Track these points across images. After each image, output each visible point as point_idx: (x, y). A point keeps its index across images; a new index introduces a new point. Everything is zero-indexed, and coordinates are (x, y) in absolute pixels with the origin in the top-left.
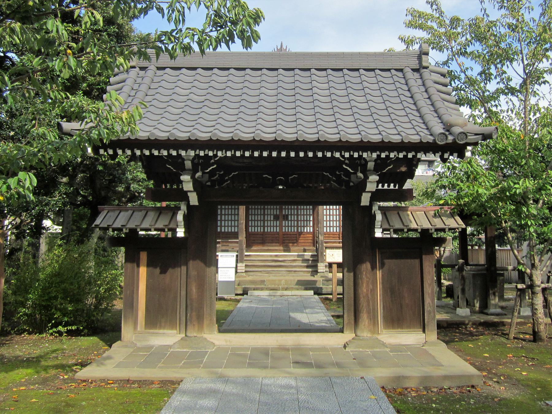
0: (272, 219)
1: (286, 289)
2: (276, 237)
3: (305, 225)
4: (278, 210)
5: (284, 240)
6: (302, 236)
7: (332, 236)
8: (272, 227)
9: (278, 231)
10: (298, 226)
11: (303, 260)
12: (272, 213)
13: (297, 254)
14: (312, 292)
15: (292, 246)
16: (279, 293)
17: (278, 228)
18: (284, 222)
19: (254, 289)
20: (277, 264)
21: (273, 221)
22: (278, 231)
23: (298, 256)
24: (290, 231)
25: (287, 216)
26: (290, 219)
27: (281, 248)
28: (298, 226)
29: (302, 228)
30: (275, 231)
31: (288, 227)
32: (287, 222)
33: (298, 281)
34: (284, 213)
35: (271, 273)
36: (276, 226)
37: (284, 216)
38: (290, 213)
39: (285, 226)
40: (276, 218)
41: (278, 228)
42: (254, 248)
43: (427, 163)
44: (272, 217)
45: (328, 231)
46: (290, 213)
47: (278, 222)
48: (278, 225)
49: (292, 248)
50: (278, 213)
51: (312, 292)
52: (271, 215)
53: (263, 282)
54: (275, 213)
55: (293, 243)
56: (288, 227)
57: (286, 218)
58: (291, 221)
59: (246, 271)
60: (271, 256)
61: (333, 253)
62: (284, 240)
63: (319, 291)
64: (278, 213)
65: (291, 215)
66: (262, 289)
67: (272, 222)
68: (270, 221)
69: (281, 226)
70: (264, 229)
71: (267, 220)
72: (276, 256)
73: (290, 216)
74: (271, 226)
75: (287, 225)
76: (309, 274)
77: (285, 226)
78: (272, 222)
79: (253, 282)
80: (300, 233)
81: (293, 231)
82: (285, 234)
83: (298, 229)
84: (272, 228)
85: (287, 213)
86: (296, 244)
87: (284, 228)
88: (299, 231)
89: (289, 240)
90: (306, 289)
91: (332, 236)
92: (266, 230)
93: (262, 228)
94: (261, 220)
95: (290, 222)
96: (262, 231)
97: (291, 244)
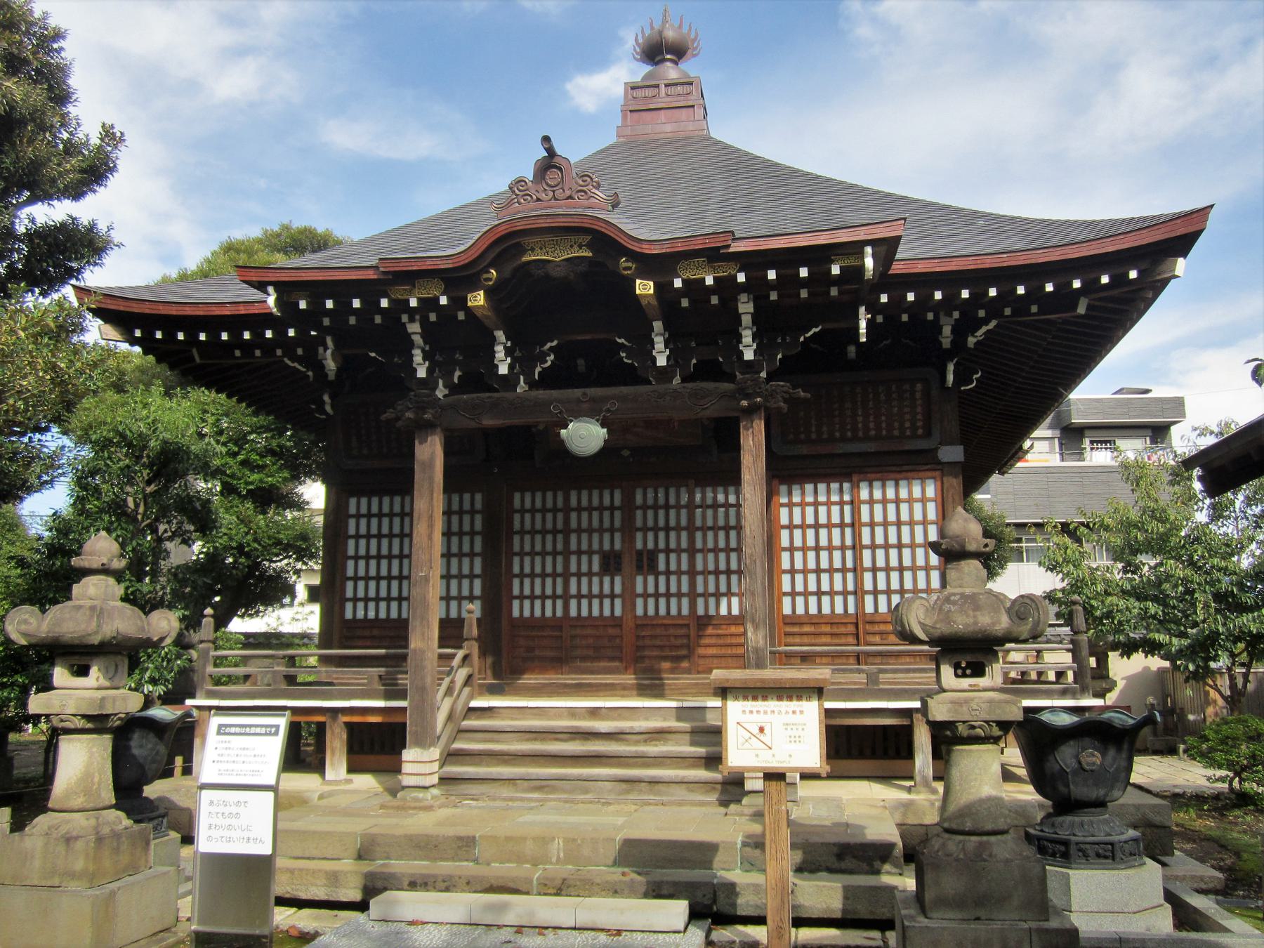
0: (596, 568)
1: (561, 889)
2: (612, 638)
3: (723, 589)
4: (617, 536)
5: (639, 648)
6: (710, 631)
7: (827, 629)
8: (596, 599)
9: (618, 612)
10: (693, 595)
11: (693, 732)
12: (596, 546)
13: (674, 704)
14: (679, 909)
15: (672, 671)
16: (520, 908)
17: (618, 602)
18: (639, 579)
19: (413, 885)
20: (590, 749)
21: (601, 575)
22: (618, 612)
23: (681, 713)
24: (662, 611)
25: (652, 556)
26: (662, 567)
27: (629, 679)
28: (693, 595)
29: (712, 601)
30: (596, 613)
31: (656, 597)
32: (651, 579)
33: (629, 844)
34: (639, 545)
35: (554, 790)
36: (612, 596)
37: (640, 554)
38: (662, 545)
39: (645, 596)
40: (611, 563)
41: (618, 602)
42: (529, 679)
43: (1149, 432)
44: (596, 559)
45: (813, 610)
46: (662, 545)
47: (618, 580)
48: (618, 590)
49: (670, 680)
50: (618, 546)
51: (679, 909)
52: (590, 553)
53: (465, 845)
54: (607, 547)
55: (678, 659)
56: (656, 597)
57: (646, 563)
58: (668, 573)
59: (444, 780)
60: (572, 713)
61: (761, 719)
62: (639, 648)
63: (722, 906)
64: (618, 546)
65: (668, 551)
66: (448, 885)
67: (596, 580)
68: (590, 574)
69: (629, 596)
70: (566, 607)
71: (579, 575)
72: (594, 713)
73: (662, 557)
74: (657, 595)
75: (651, 590)
76: (713, 797)
77: (645, 596)
78: (596, 580)
79: (425, 846)
80: (704, 622)
81: (674, 611)
82: (645, 623)
83: (693, 606)
84: (607, 602)
85: (650, 545)
86: (685, 664)
87: (640, 602)
88: (701, 612)
89: (661, 647)
90: (658, 891)
91: (827, 629)
92: (573, 612)
93: (559, 603)
94: (554, 575)
95: (662, 579)
96: (559, 613)
97: (666, 665)
